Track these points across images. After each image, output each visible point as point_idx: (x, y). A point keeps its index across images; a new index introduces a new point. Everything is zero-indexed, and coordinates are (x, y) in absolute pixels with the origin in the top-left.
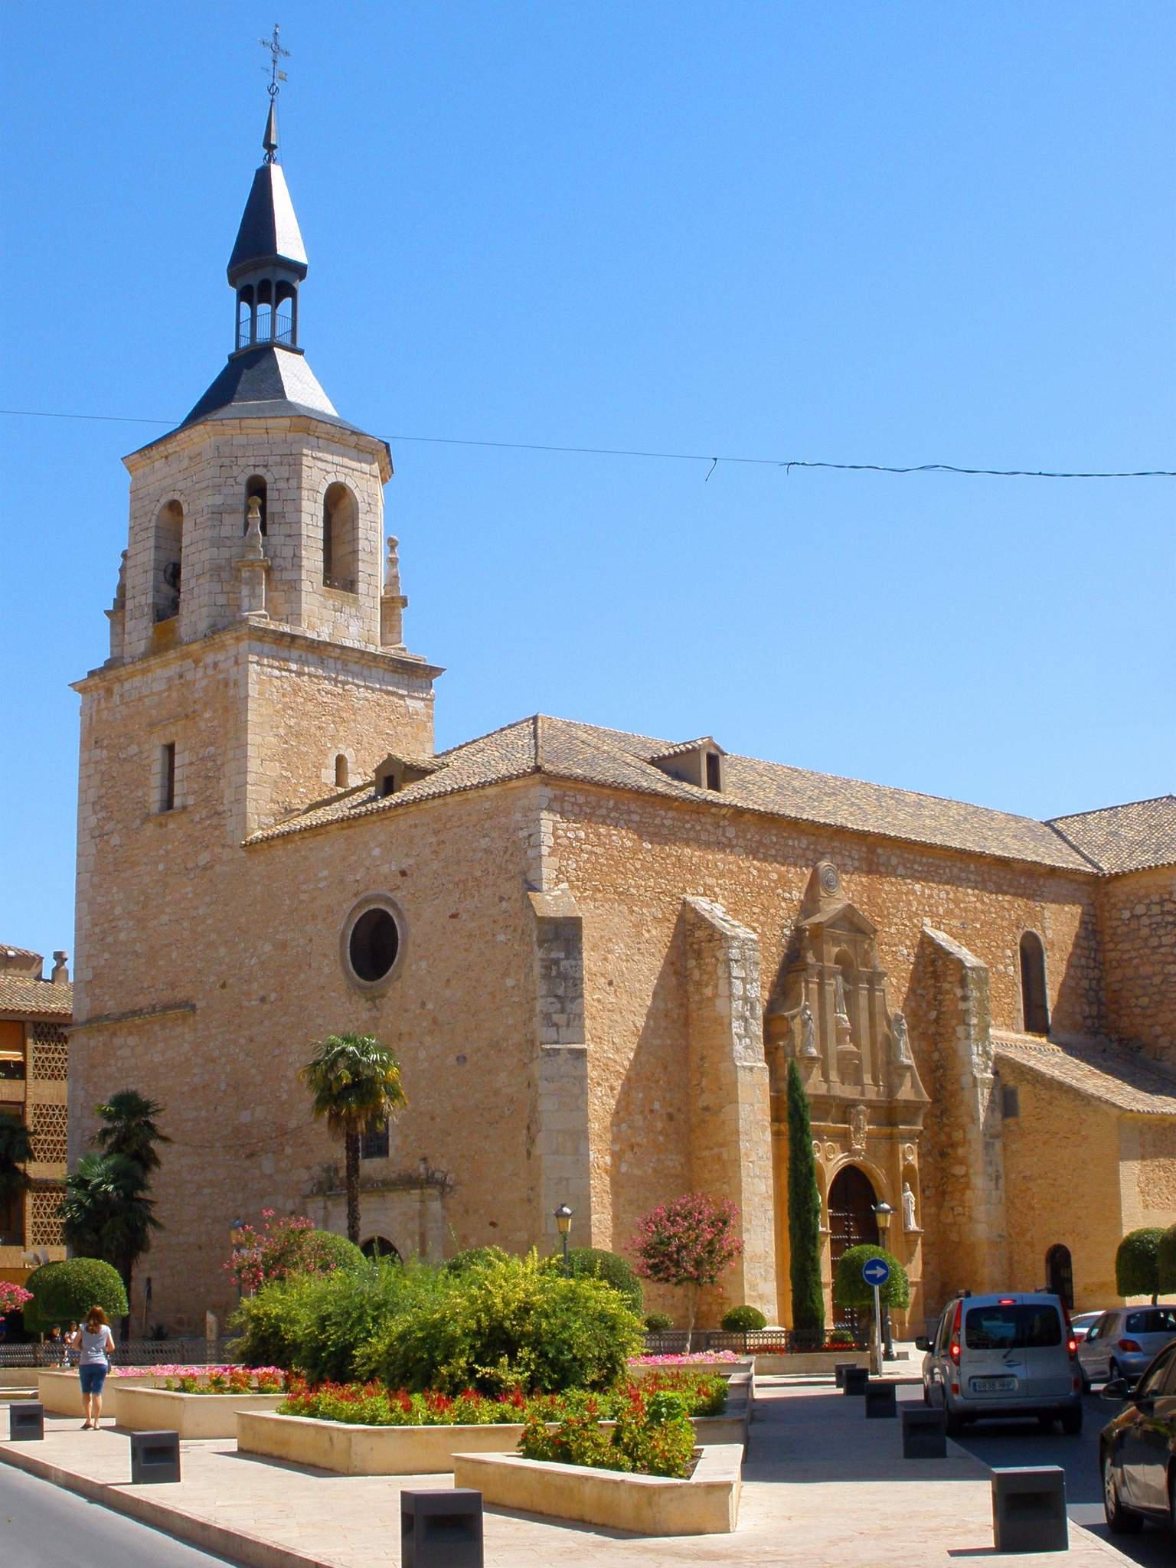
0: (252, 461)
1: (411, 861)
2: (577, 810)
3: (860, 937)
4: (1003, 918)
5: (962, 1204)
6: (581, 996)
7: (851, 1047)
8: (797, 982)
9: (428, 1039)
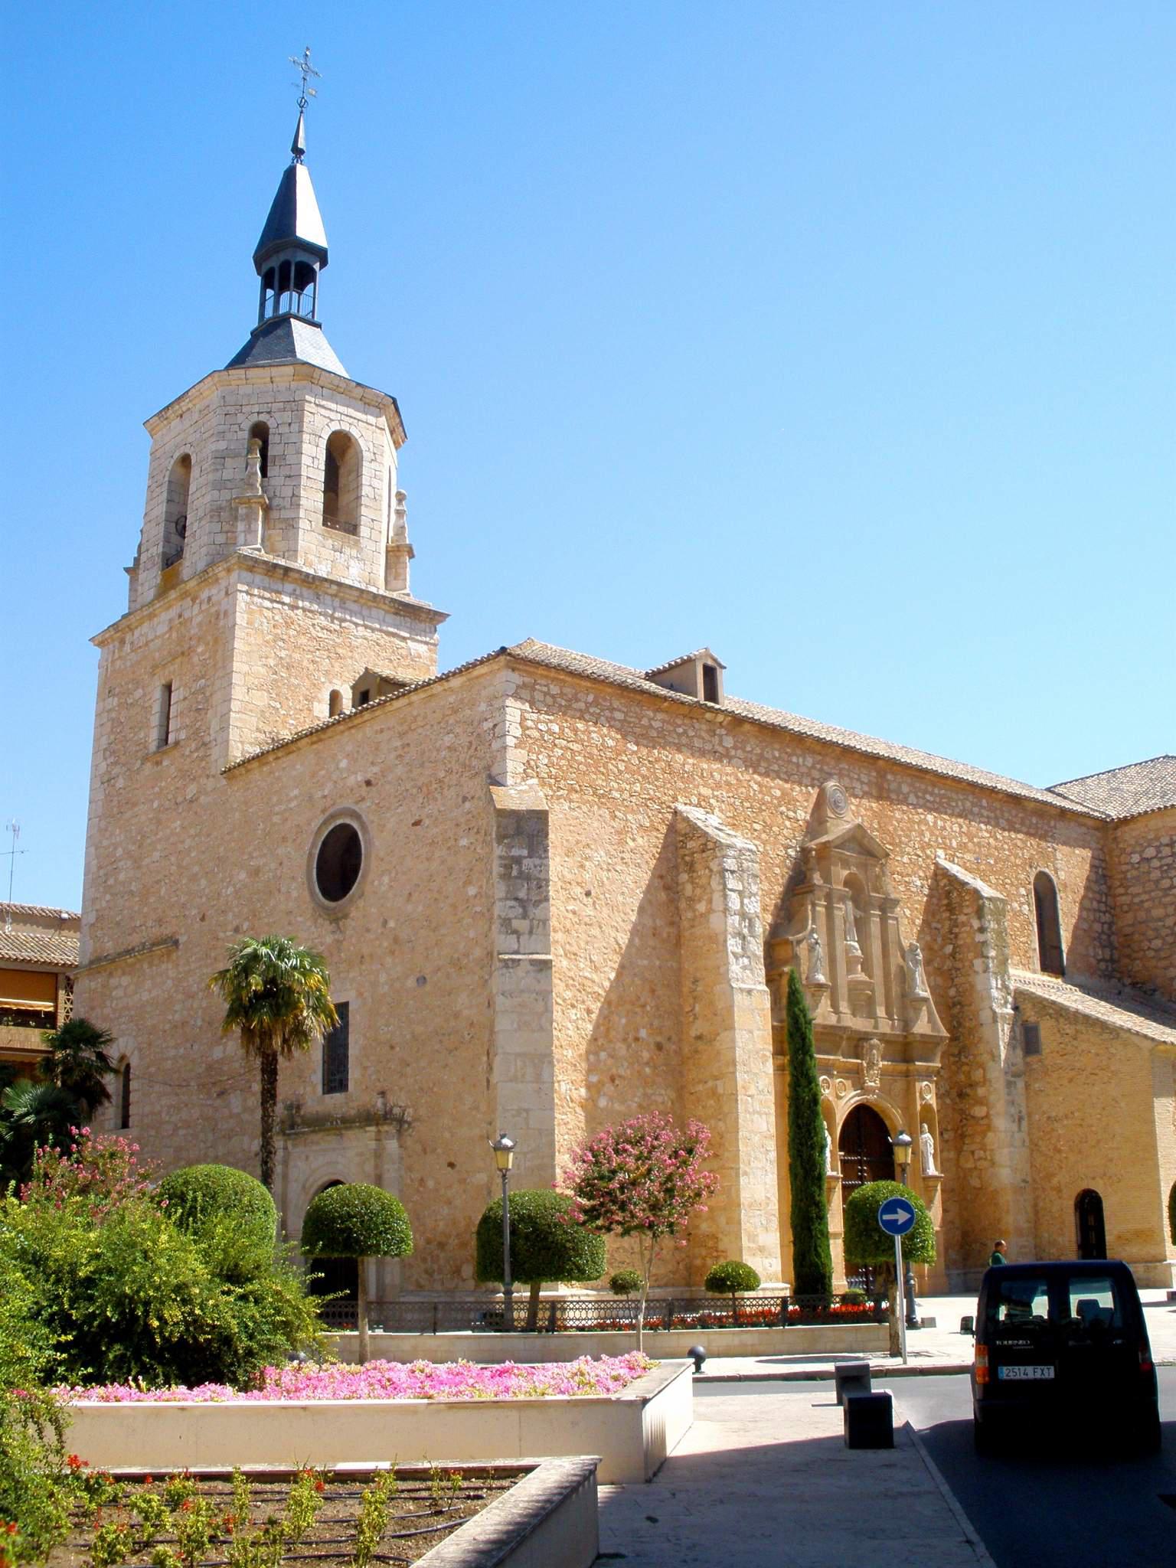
0: (256, 409)
1: (375, 769)
2: (549, 700)
3: (871, 861)
4: (1016, 856)
5: (984, 1148)
6: (547, 899)
7: (861, 976)
9: (389, 960)
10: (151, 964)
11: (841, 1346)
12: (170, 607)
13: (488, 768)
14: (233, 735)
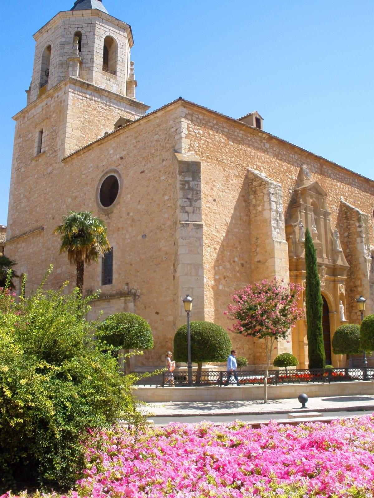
0: (77, 26)
1: (125, 152)
2: (199, 121)
3: (320, 197)
4: (367, 202)
6: (200, 199)
8: (296, 211)
9: (130, 229)
10: (33, 238)
11: (356, 392)
12: (43, 101)
13: (174, 147)
14: (67, 146)
